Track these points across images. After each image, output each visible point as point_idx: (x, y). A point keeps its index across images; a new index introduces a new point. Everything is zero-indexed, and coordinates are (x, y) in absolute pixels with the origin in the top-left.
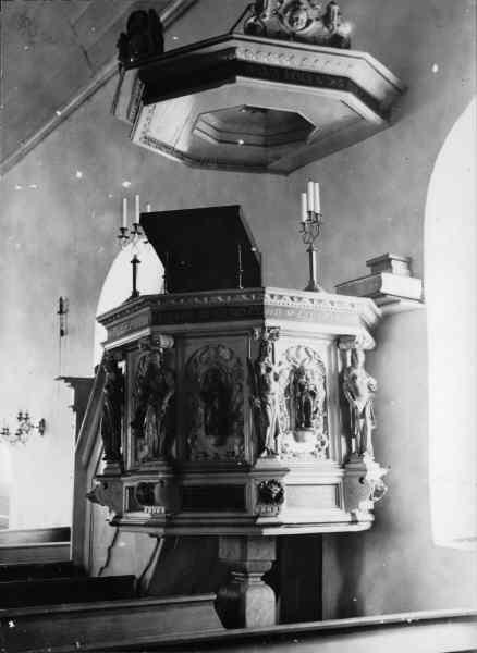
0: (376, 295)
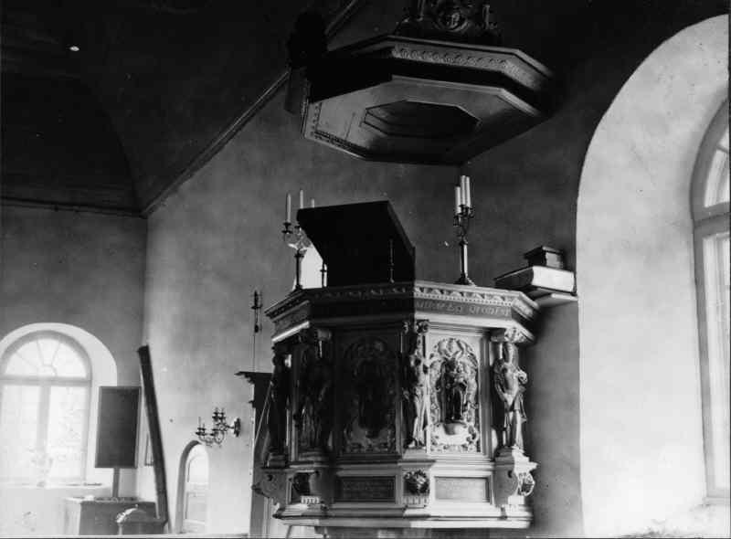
0: (529, 289)
